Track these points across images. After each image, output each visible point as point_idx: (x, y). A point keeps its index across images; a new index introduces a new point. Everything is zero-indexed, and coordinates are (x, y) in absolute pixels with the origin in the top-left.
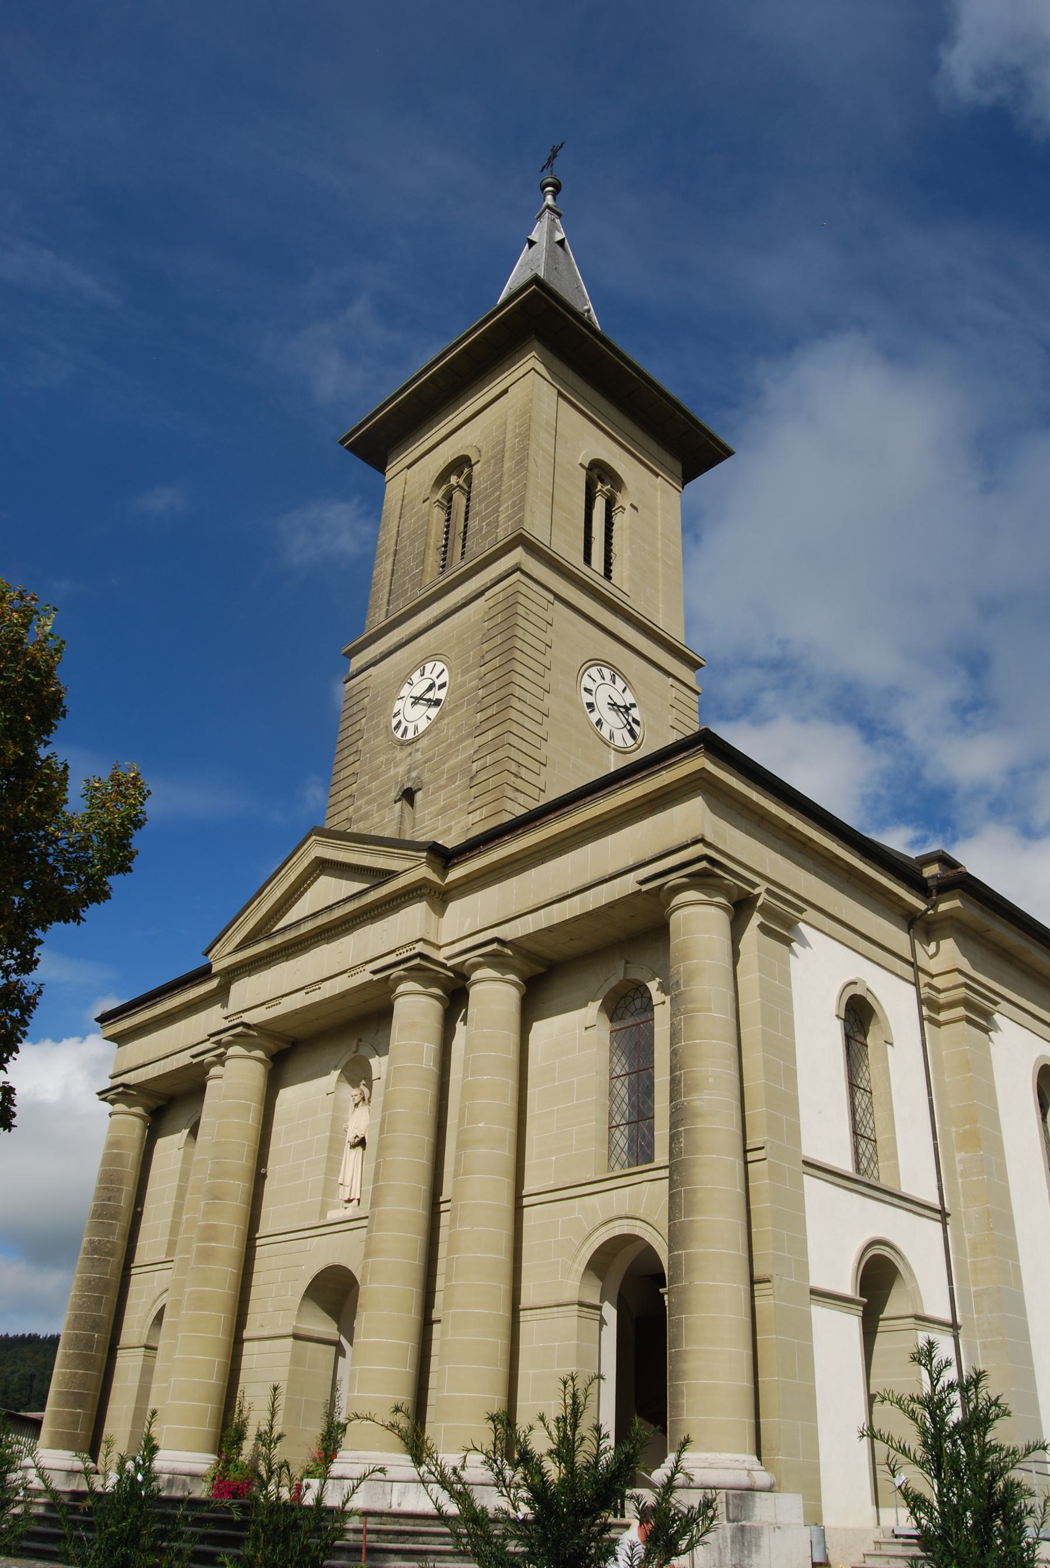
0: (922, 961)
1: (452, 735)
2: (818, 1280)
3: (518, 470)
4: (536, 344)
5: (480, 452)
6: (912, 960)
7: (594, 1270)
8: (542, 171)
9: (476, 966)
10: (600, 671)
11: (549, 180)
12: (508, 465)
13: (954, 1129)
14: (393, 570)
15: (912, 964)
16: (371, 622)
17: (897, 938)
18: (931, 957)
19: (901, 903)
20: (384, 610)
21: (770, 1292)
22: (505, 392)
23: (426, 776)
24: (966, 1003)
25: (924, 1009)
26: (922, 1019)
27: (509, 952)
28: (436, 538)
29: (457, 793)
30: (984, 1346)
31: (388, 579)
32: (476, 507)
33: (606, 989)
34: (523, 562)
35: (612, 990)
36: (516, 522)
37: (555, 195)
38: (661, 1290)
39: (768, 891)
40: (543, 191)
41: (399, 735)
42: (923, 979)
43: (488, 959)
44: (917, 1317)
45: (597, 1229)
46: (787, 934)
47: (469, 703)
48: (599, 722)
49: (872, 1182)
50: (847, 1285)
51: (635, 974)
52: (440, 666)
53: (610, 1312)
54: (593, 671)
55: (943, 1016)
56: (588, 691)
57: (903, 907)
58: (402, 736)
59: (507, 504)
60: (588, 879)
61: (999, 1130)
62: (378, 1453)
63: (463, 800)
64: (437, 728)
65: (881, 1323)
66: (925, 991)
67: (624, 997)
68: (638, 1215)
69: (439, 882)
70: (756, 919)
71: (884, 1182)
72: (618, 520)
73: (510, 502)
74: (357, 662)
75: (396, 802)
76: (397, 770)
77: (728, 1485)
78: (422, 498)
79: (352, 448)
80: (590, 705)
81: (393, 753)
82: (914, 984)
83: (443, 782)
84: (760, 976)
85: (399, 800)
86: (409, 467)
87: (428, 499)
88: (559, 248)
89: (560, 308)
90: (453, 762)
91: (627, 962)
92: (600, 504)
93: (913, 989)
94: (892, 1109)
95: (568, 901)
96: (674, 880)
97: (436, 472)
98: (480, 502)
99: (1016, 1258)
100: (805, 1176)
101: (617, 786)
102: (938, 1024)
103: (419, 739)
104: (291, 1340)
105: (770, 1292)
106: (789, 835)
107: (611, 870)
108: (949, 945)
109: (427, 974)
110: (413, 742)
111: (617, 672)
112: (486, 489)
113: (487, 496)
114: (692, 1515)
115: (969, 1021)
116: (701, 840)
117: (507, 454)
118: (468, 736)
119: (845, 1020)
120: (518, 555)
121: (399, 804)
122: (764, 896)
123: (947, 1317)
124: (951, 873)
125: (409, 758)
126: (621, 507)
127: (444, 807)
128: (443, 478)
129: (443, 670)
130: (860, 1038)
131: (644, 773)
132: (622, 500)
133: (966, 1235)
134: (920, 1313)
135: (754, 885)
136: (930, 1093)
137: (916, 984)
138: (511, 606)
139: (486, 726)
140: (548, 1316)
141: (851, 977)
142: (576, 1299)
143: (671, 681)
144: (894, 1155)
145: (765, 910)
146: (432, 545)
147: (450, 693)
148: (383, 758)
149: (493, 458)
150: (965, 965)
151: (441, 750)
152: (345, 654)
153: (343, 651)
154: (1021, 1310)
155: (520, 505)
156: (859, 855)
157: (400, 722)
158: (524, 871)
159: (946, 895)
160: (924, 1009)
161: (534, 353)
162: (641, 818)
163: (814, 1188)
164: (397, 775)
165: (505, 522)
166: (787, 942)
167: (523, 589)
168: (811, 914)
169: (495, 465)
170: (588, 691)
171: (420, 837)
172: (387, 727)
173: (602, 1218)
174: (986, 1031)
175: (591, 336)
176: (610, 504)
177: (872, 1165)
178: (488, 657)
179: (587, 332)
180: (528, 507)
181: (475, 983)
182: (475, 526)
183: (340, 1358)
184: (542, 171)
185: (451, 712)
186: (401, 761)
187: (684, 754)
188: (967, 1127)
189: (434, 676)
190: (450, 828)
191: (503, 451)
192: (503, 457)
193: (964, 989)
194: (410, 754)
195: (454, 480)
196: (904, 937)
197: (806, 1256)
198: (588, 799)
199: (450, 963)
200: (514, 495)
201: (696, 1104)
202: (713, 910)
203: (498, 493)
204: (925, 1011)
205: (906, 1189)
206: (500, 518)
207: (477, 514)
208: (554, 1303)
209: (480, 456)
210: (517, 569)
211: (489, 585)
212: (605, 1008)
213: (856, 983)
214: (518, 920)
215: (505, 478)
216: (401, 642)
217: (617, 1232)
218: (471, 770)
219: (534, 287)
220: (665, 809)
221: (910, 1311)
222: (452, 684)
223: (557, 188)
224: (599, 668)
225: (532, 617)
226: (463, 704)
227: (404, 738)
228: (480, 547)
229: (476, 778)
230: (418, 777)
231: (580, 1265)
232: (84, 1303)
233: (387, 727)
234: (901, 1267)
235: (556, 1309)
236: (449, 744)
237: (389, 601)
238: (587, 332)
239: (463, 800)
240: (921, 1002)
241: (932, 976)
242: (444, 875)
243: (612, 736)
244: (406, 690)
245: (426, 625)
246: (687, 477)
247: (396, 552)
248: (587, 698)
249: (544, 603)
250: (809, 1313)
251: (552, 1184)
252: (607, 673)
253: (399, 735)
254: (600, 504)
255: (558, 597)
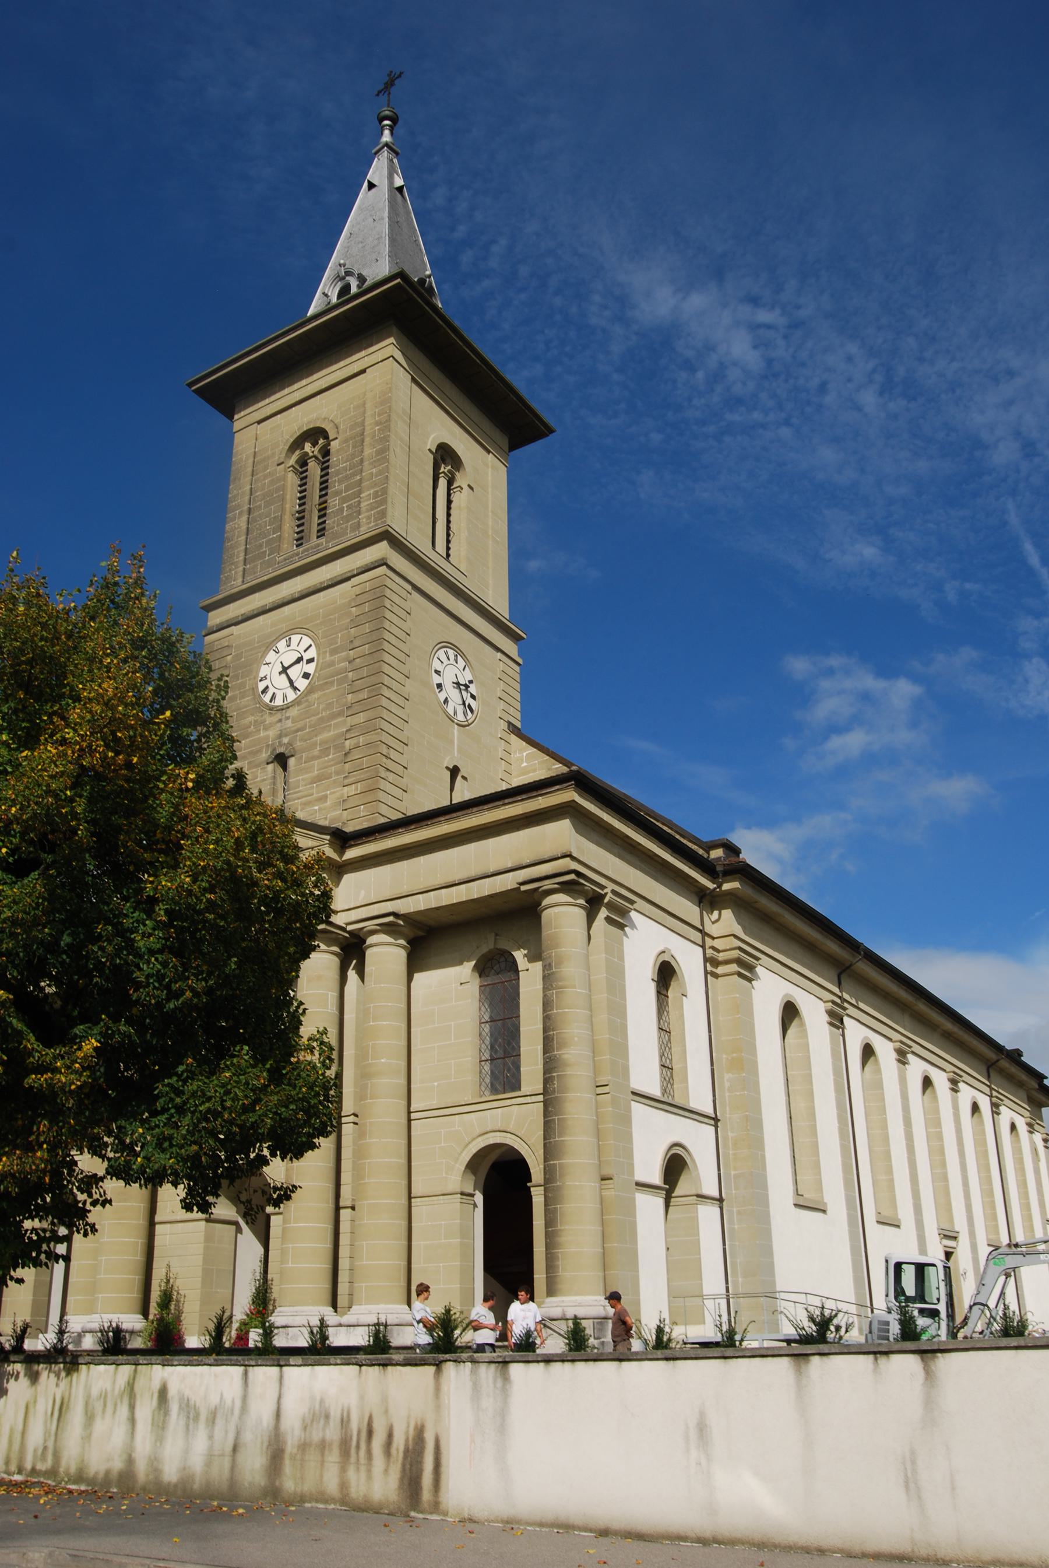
0: (709, 928)
1: (323, 710)
2: (640, 1177)
3: (378, 460)
4: (395, 330)
6: (701, 928)
7: (468, 1170)
8: (378, 95)
9: (373, 932)
10: (446, 653)
11: (387, 113)
12: (368, 451)
13: (724, 1056)
14: (248, 528)
15: (700, 931)
16: (227, 578)
17: (688, 909)
18: (713, 923)
19: (696, 884)
20: (241, 569)
21: (612, 1186)
22: (363, 371)
23: (298, 744)
24: (739, 962)
25: (708, 965)
26: (706, 973)
27: (402, 923)
28: (291, 504)
29: (332, 766)
30: (739, 1213)
31: (243, 538)
32: (336, 485)
33: (478, 954)
34: (388, 556)
35: (483, 955)
36: (378, 513)
37: (392, 129)
38: (528, 1184)
39: (614, 892)
40: (380, 124)
41: (267, 698)
42: (708, 941)
43: (384, 928)
44: (699, 1196)
45: (474, 1139)
46: (622, 921)
47: (340, 682)
48: (446, 701)
49: (670, 1100)
50: (656, 1177)
51: (503, 945)
52: (307, 641)
53: (479, 1198)
54: (441, 654)
55: (720, 970)
56: (437, 672)
57: (696, 887)
58: (271, 701)
59: (368, 492)
60: (473, 873)
61: (755, 1055)
62: (311, 1308)
63: (337, 773)
65: (673, 1200)
66: (709, 952)
67: (492, 959)
68: (509, 1130)
69: (338, 859)
70: (603, 913)
71: (678, 1101)
72: (455, 498)
73: (372, 491)
74: (216, 618)
75: (268, 764)
76: (267, 733)
77: (592, 1316)
78: (276, 459)
79: (199, 392)
80: (439, 686)
81: (262, 716)
82: (702, 947)
83: (316, 752)
84: (606, 958)
85: (272, 762)
86: (259, 422)
87: (283, 463)
88: (399, 195)
90: (326, 735)
91: (496, 935)
92: (443, 483)
93: (700, 950)
94: (684, 1045)
95: (454, 888)
96: (547, 885)
97: (291, 437)
98: (340, 482)
99: (763, 1150)
100: (633, 1102)
101: (501, 803)
102: (716, 976)
103: (288, 708)
104: (204, 1222)
105: (612, 1186)
106: (625, 841)
107: (492, 869)
108: (727, 914)
109: (328, 935)
110: (281, 709)
111: (459, 652)
113: (347, 478)
115: (740, 975)
116: (569, 856)
117: (367, 440)
118: (340, 714)
120: (384, 545)
121: (270, 767)
122: (610, 895)
123: (716, 1194)
124: (733, 859)
125: (279, 725)
126: (459, 487)
127: (318, 776)
128: (297, 444)
129: (311, 646)
130: (664, 992)
131: (524, 797)
132: (461, 480)
133: (730, 1134)
134: (700, 1193)
135: (603, 887)
136: (710, 1031)
137: (703, 946)
138: (377, 598)
139: (356, 708)
140: (435, 1202)
141: (661, 948)
142: (459, 1190)
143: (499, 655)
144: (685, 1080)
145: (611, 906)
146: (288, 509)
147: (319, 669)
148: (251, 718)
149: (351, 438)
150: (739, 931)
151: (313, 723)
152: (203, 608)
153: (201, 605)
154: (765, 1187)
155: (381, 498)
156: (670, 851)
157: (267, 687)
158: (414, 857)
159: (729, 878)
160: (708, 965)
161: (392, 340)
162: (518, 829)
163: (639, 1111)
164: (267, 737)
165: (368, 511)
166: (621, 927)
167: (389, 583)
168: (640, 904)
169: (354, 447)
170: (437, 672)
172: (254, 688)
173: (478, 1131)
174: (750, 980)
175: (444, 325)
176: (450, 483)
177: (669, 1085)
178: (357, 643)
179: (441, 322)
180: (389, 500)
181: (371, 946)
182: (335, 506)
183: (239, 1235)
184: (378, 95)
185: (321, 688)
186: (271, 725)
187: (558, 787)
188: (734, 1055)
189: (302, 648)
190: (326, 797)
191: (362, 434)
192: (363, 441)
193: (738, 952)
194: (280, 721)
195: (308, 447)
196: (697, 909)
197: (633, 1160)
198: (475, 809)
199: (349, 928)
200: (375, 485)
201: (565, 1056)
202: (577, 910)
203: (358, 478)
204: (709, 968)
205: (693, 1105)
206: (362, 505)
207: (337, 493)
208: (440, 1193)
209: (338, 432)
210: (383, 563)
211: (355, 572)
212: (476, 968)
213: (664, 952)
214: (409, 898)
215: (366, 463)
216: (264, 609)
217: (491, 1141)
218: (344, 747)
219: (399, 280)
220: (538, 825)
221: (694, 1192)
222: (321, 661)
223: (394, 120)
224: (445, 649)
225: (396, 609)
226: (332, 683)
227: (272, 704)
229: (349, 755)
230: (290, 744)
231: (461, 1166)
233: (253, 689)
234: (688, 1160)
235: (442, 1197)
236: (319, 719)
237: (245, 560)
238: (441, 322)
239: (337, 773)
240: (706, 960)
241: (713, 938)
242: (341, 853)
243: (455, 713)
244: (271, 656)
245: (290, 598)
246: (513, 447)
247: (250, 511)
248: (437, 680)
249: (404, 594)
250: (633, 1200)
251: (435, 1103)
252: (451, 653)
253: (267, 698)
254: (443, 483)
255: (416, 588)
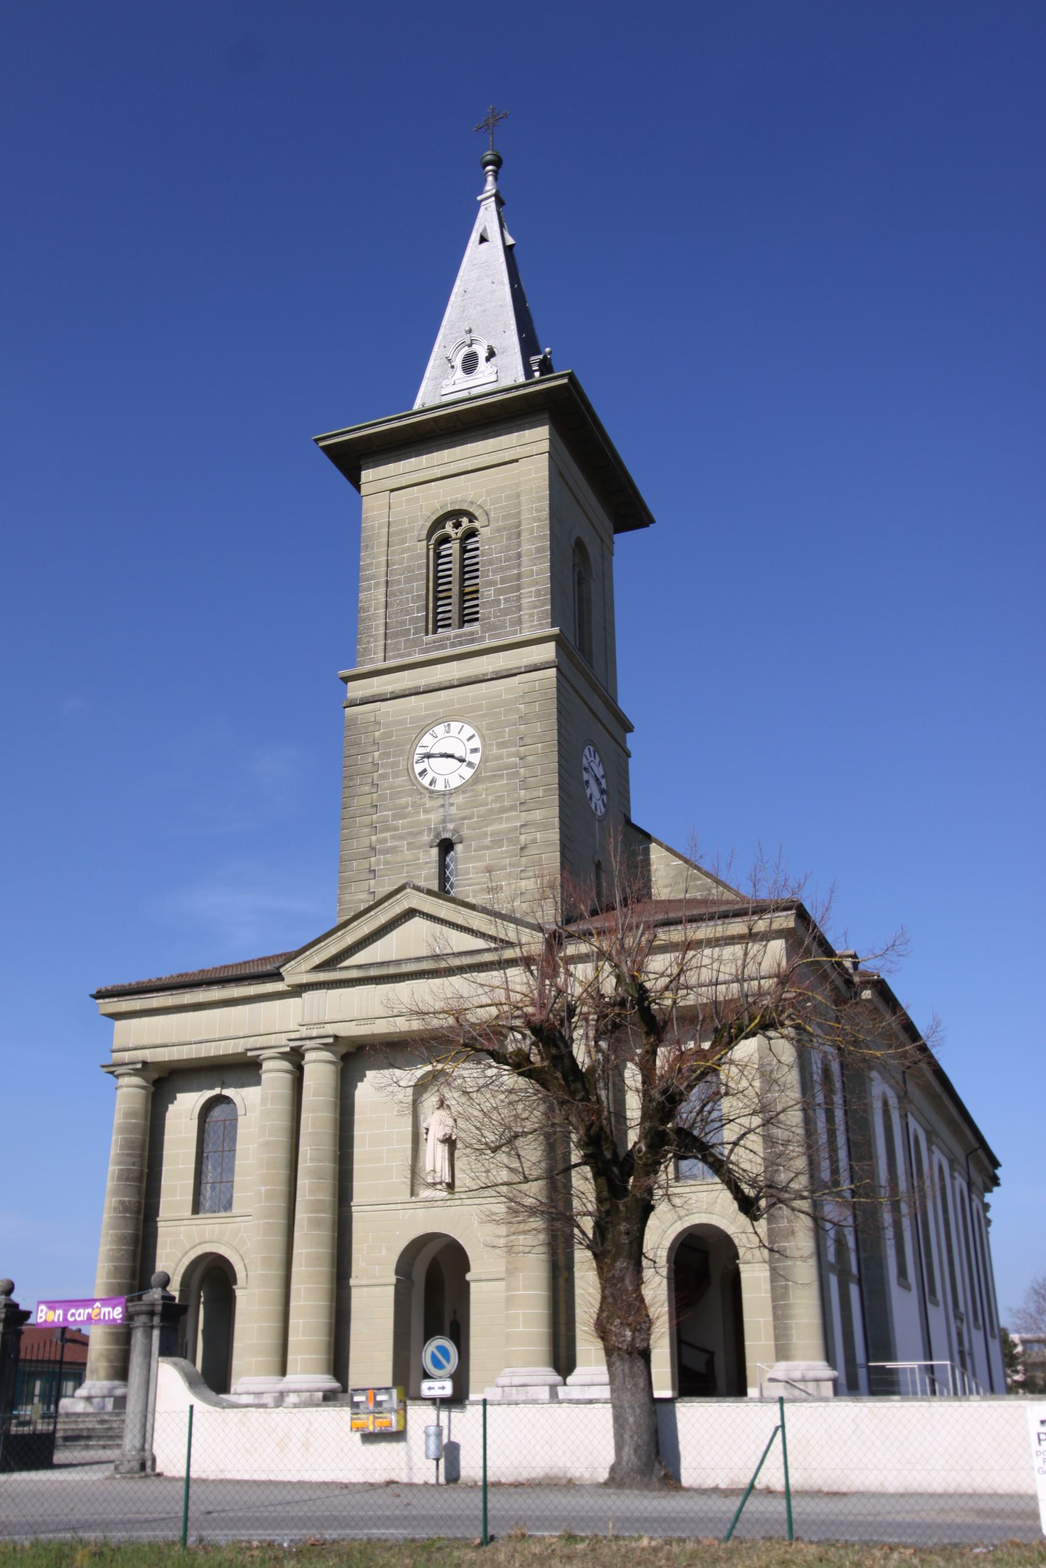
5: (487, 515)
29: (506, 858)
59: (530, 590)
63: (511, 865)
64: (472, 790)
89: (583, 407)
112: (499, 560)
114: (481, 877)
119: (768, 941)
171: (465, 886)
194: (443, 806)
195: (449, 528)
223: (498, 163)
226: (502, 776)
228: (499, 621)
232: (122, 1255)
